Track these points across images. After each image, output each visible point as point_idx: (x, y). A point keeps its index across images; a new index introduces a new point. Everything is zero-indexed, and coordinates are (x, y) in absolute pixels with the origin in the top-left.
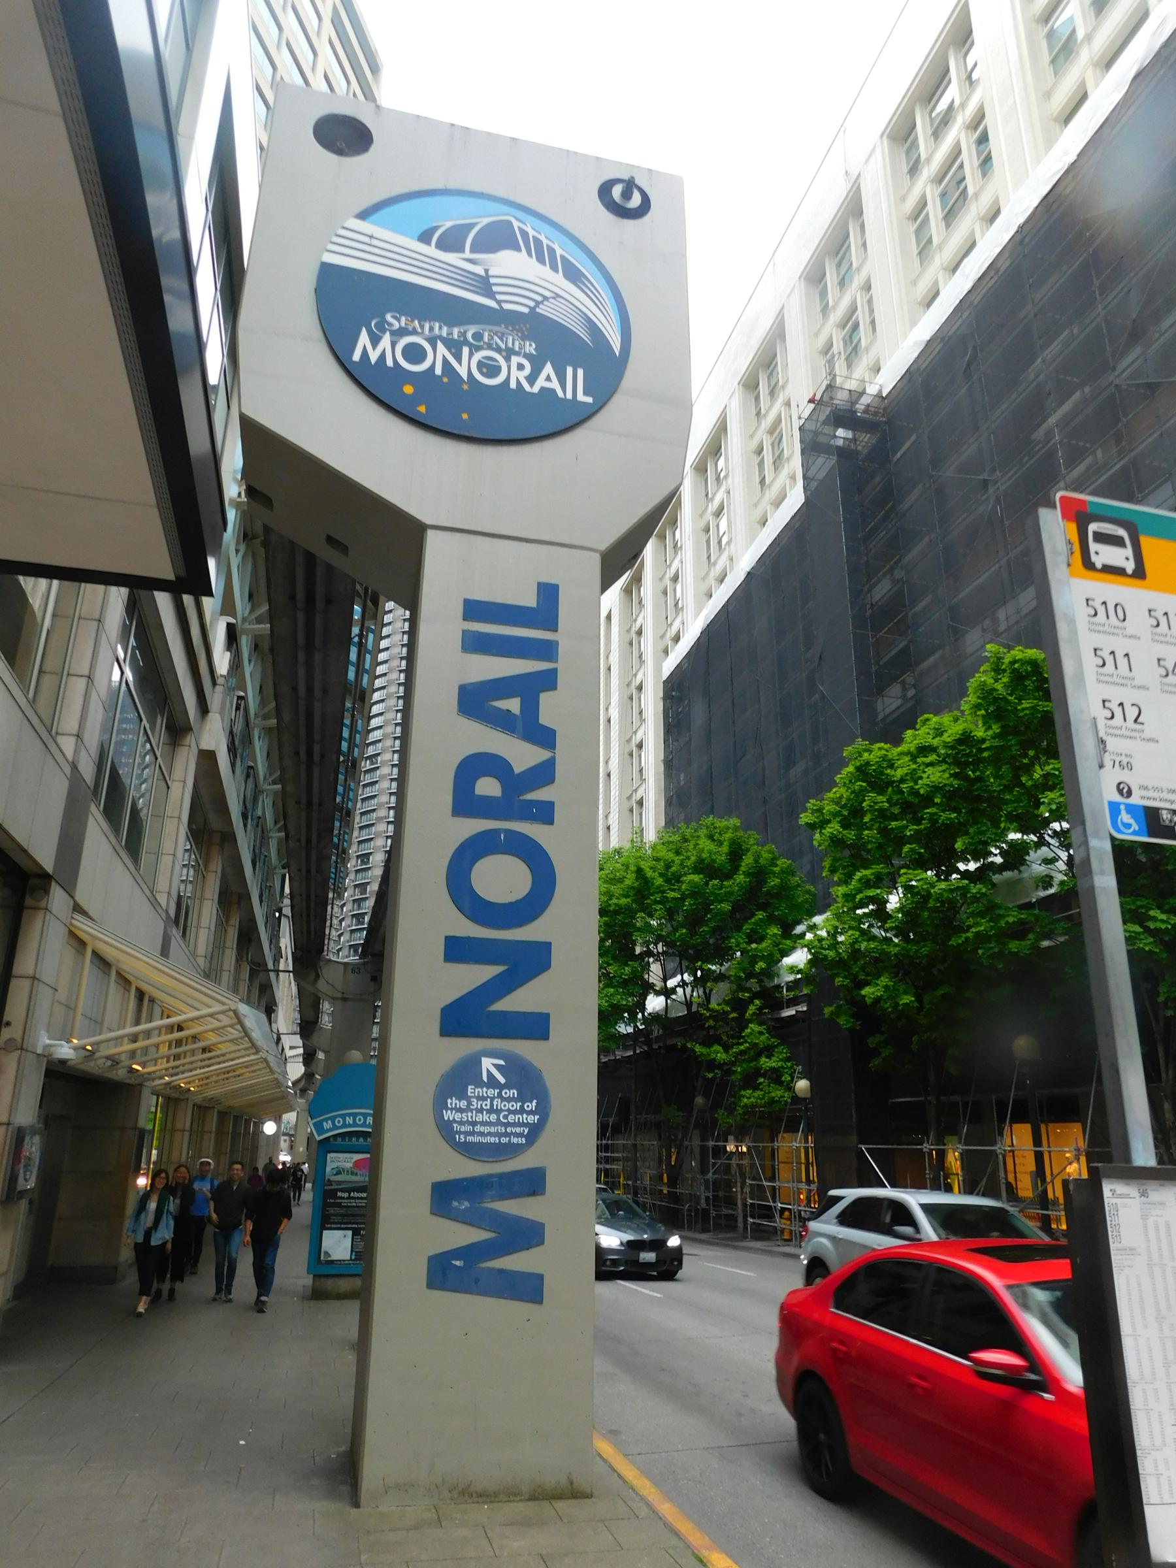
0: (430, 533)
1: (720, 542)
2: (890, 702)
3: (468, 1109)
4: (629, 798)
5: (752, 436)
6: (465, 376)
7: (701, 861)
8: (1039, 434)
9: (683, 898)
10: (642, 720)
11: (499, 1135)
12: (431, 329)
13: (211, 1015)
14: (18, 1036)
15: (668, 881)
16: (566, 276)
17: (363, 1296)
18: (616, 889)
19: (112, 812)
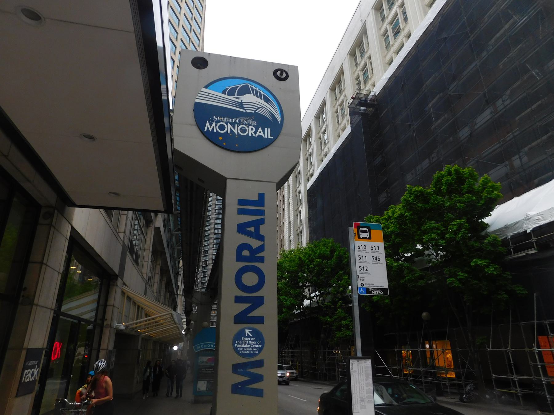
0: (228, 180)
1: (325, 142)
2: (383, 198)
3: (242, 344)
4: (297, 230)
5: (334, 107)
6: (236, 133)
7: (320, 254)
8: (427, 109)
9: (315, 267)
10: (301, 204)
11: (251, 351)
12: (226, 120)
13: (165, 315)
14: (109, 323)
15: (310, 261)
16: (265, 101)
17: (213, 402)
18: (292, 264)
19: (131, 252)
